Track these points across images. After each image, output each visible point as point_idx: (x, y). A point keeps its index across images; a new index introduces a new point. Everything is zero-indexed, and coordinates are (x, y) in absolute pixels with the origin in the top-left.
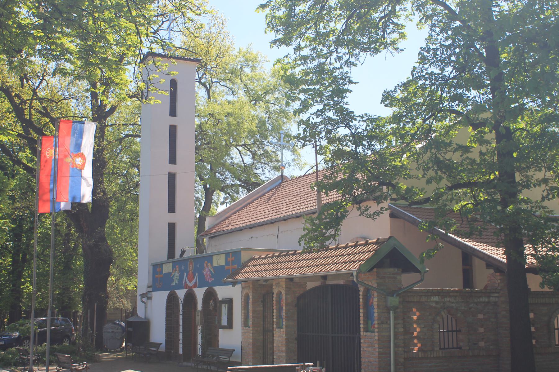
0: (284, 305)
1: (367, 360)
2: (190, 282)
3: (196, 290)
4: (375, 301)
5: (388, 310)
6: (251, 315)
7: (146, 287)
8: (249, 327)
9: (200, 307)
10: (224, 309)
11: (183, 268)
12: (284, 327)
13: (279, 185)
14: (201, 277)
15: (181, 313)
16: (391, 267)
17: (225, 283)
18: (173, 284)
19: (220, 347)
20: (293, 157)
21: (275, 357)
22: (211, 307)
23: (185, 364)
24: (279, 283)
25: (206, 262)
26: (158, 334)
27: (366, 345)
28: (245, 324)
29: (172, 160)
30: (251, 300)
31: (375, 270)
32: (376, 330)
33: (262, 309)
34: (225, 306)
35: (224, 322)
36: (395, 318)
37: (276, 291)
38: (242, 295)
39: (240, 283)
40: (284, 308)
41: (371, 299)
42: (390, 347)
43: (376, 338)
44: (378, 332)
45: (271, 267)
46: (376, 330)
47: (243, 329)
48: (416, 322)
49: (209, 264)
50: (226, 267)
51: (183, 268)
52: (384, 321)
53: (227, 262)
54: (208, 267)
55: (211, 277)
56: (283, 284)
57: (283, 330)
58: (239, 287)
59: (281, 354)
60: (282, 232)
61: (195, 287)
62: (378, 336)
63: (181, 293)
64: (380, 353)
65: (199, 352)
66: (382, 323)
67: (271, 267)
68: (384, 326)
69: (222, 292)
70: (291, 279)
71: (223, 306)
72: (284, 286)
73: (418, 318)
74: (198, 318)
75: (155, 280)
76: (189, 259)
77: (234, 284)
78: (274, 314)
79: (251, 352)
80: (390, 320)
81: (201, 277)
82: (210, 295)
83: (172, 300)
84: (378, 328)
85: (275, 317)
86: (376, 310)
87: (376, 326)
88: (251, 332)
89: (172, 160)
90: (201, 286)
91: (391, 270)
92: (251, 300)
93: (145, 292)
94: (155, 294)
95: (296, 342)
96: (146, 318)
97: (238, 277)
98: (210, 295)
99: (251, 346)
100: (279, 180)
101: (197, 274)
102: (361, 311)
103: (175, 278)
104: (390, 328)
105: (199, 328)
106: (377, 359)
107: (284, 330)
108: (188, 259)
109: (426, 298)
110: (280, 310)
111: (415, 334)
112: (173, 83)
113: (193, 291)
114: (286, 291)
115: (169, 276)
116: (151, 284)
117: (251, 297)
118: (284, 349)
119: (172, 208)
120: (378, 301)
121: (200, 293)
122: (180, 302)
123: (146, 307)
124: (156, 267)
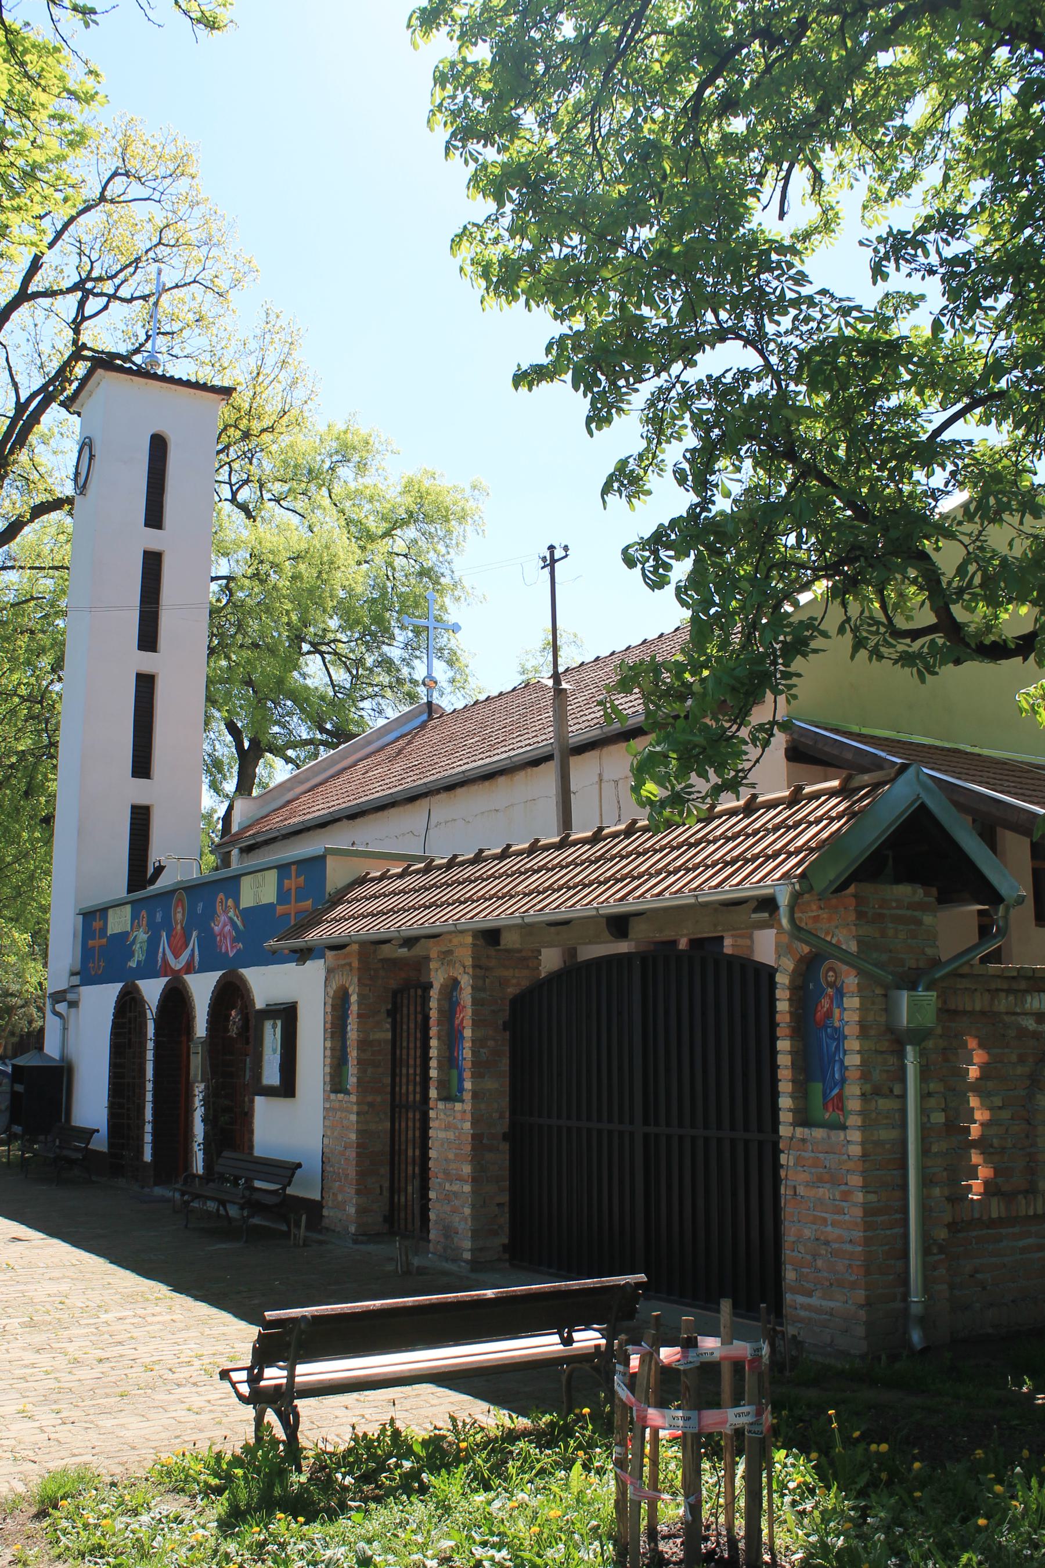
0: (468, 1022)
1: (807, 1233)
2: (177, 956)
3: (189, 979)
4: (850, 1012)
5: (897, 1041)
6: (353, 1054)
7: (66, 974)
8: (347, 1092)
9: (201, 1028)
10: (272, 1036)
11: (159, 917)
12: (467, 1096)
13: (423, 726)
14: (208, 942)
15: (150, 1045)
16: (898, 880)
17: (274, 952)
18: (133, 964)
19: (257, 1152)
20: (450, 674)
21: (432, 1195)
22: (233, 1031)
23: (158, 1191)
24: (450, 952)
25: (221, 896)
26: (91, 1105)
27: (803, 1177)
28: (336, 1084)
29: (148, 640)
30: (354, 1008)
31: (852, 889)
32: (854, 1120)
33: (389, 1035)
34: (274, 1027)
35: (271, 1075)
36: (924, 1074)
37: (438, 978)
38: (326, 993)
39: (322, 956)
40: (468, 1033)
41: (825, 1003)
42: (905, 1187)
43: (855, 1150)
44: (863, 1128)
45: (425, 898)
46: (854, 1120)
47: (326, 1099)
48: (977, 1088)
49: (230, 902)
50: (280, 909)
51: (159, 917)
52: (885, 1086)
53: (283, 895)
54: (226, 911)
55: (234, 940)
56: (465, 954)
57: (464, 1107)
58: (315, 968)
59: (455, 1188)
60: (438, 824)
61: (188, 972)
62: (863, 1143)
63: (152, 990)
64: (869, 1211)
65: (199, 1165)
66: (877, 1092)
67: (425, 898)
68: (884, 1104)
69: (266, 984)
70: (491, 936)
71: (268, 1025)
72: (469, 962)
73: (984, 1076)
74: (197, 1062)
75: (87, 954)
76: (174, 891)
77: (303, 955)
78: (433, 1053)
79: (352, 1172)
80: (903, 1080)
81: (208, 942)
82: (231, 994)
83: (129, 1005)
84: (862, 1113)
85: (433, 1063)
86: (853, 1044)
87: (854, 1104)
88: (355, 1108)
89: (148, 640)
90: (204, 968)
91: (904, 891)
92: (354, 1008)
93: (64, 986)
94: (88, 993)
95: (505, 1147)
96: (63, 1058)
97: (316, 935)
98: (231, 994)
99: (352, 1154)
100: (421, 713)
101: (195, 934)
102: (783, 1045)
103: (137, 947)
104: (904, 1111)
105: (199, 1090)
106: (858, 1234)
107: (468, 1106)
108: (168, 894)
109: (1011, 998)
110: (452, 1038)
111: (975, 1131)
112: (159, 446)
113: (184, 983)
114: (474, 977)
115: (122, 942)
116: (78, 967)
117: (354, 998)
118: (467, 1169)
119: (142, 766)
120: (863, 1009)
121: (202, 988)
122: (149, 1016)
123: (65, 1029)
124: (92, 917)
